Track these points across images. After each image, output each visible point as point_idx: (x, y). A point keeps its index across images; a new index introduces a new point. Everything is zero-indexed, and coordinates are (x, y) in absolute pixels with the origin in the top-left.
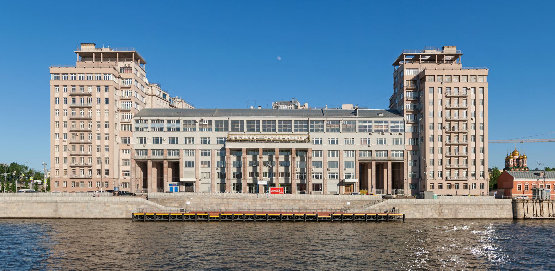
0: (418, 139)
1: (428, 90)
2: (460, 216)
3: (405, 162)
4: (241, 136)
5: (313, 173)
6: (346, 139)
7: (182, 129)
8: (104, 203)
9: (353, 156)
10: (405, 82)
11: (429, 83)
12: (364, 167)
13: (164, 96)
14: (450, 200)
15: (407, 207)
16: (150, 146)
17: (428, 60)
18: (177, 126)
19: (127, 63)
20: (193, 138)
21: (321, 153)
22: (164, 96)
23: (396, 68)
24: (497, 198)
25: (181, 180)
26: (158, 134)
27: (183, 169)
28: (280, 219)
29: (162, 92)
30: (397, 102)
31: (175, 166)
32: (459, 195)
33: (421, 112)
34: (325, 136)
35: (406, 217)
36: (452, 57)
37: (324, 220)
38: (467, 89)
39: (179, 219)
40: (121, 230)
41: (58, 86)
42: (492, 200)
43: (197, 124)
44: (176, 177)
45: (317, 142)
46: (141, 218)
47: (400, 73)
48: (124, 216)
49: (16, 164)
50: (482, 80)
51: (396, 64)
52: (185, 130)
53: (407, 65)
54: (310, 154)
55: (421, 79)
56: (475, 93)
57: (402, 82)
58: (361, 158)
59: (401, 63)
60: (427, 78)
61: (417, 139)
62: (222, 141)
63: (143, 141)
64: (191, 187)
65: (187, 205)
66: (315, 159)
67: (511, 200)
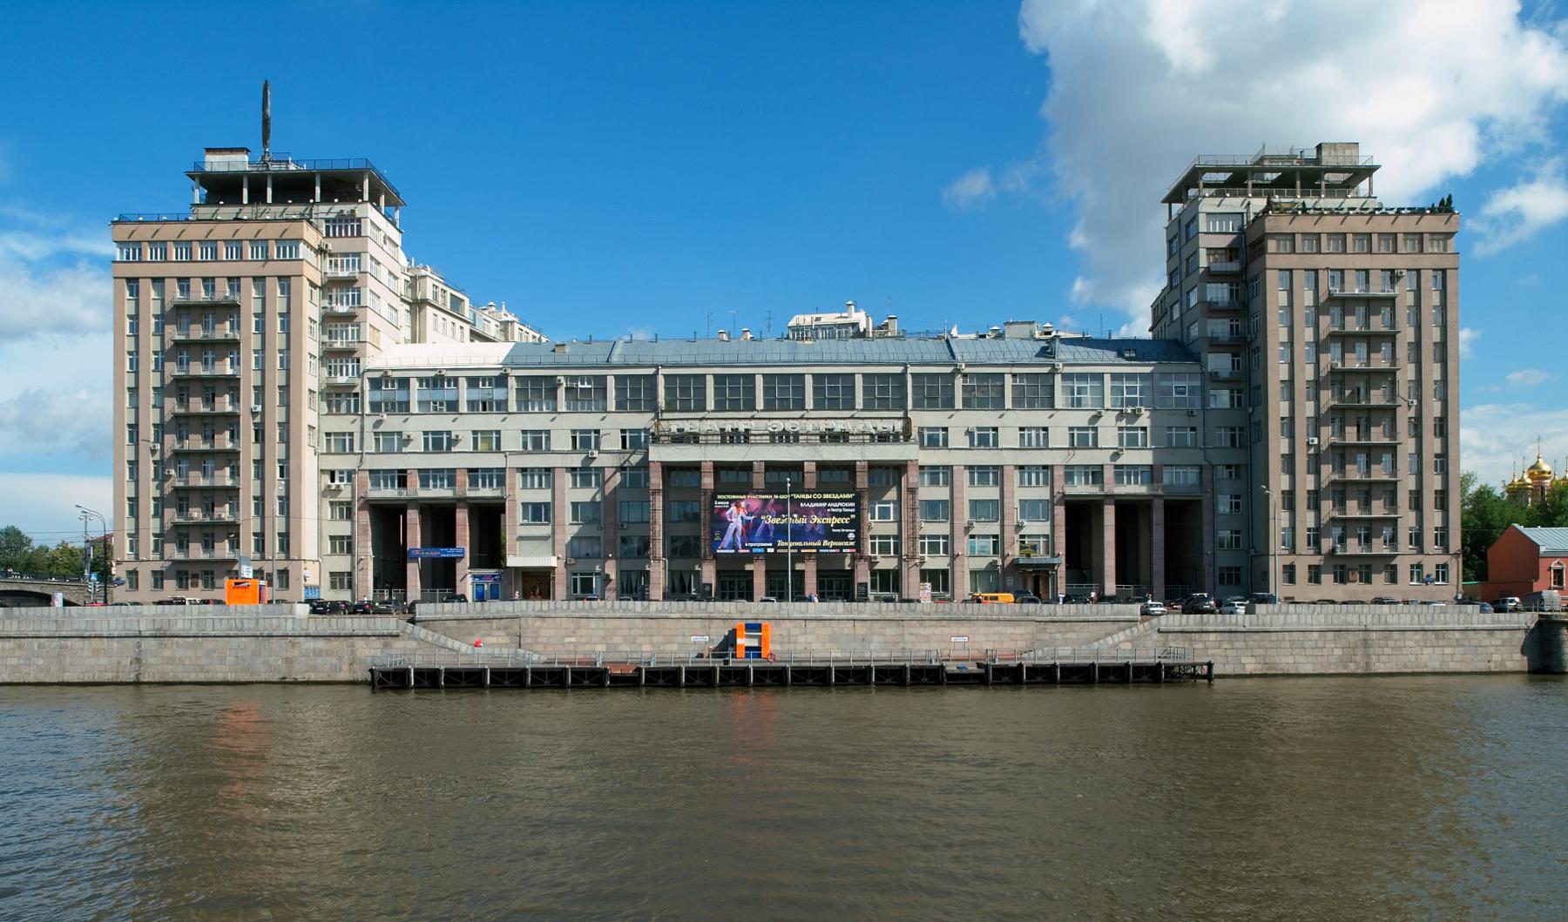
0: (1002, 526)
1: (1273, 279)
2: (1380, 667)
3: (242, 376)
4: (681, 424)
5: (923, 537)
6: (1022, 429)
7: (513, 407)
8: (1236, 901)
9: (1046, 483)
10: (1203, 253)
11: (1275, 258)
12: (1081, 515)
13: (456, 302)
14: (1349, 618)
15: (1220, 640)
16: (414, 460)
17: (1226, 184)
18: (498, 394)
19: (346, 208)
20: (498, 432)
21: (945, 545)
22: (456, 302)
23: (1177, 207)
24: (1184, 612)
25: (512, 561)
26: (442, 422)
27: (515, 525)
28: (854, 677)
29: (449, 291)
30: (1176, 315)
31: (489, 517)
32: (554, 453)
33: (1254, 345)
34: (960, 422)
35: (1216, 671)
36: (1347, 176)
37: (962, 680)
38: (234, 281)
39: (510, 680)
40: (316, 719)
41: (162, 279)
42: (1474, 615)
43: (561, 393)
44: (490, 549)
45: (933, 443)
46: (391, 680)
47: (1187, 226)
48: (344, 676)
49: (19, 533)
50: (217, 626)
51: (1177, 195)
52: (523, 404)
53: (1208, 204)
54: (912, 477)
55: (1253, 245)
56: (266, 122)
57: (1196, 253)
58: (1070, 491)
59: (1192, 192)
60: (1271, 245)
61: (1241, 429)
62: (632, 441)
63: (984, 438)
64: (1032, 595)
65: (698, 574)
66: (928, 493)
67: (1528, 619)
